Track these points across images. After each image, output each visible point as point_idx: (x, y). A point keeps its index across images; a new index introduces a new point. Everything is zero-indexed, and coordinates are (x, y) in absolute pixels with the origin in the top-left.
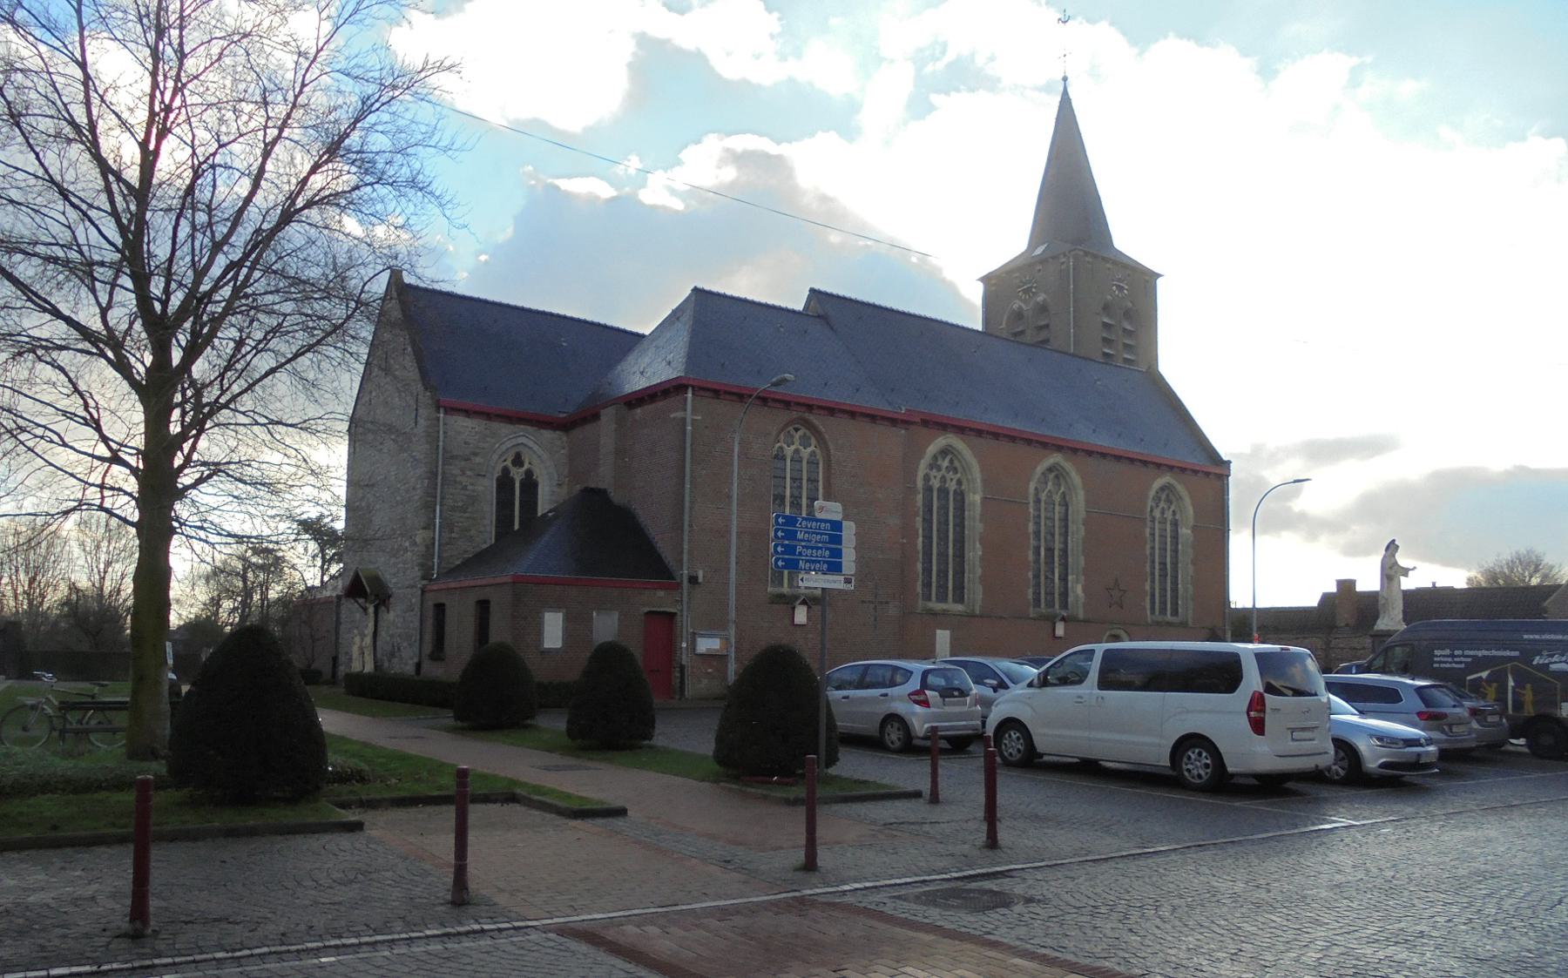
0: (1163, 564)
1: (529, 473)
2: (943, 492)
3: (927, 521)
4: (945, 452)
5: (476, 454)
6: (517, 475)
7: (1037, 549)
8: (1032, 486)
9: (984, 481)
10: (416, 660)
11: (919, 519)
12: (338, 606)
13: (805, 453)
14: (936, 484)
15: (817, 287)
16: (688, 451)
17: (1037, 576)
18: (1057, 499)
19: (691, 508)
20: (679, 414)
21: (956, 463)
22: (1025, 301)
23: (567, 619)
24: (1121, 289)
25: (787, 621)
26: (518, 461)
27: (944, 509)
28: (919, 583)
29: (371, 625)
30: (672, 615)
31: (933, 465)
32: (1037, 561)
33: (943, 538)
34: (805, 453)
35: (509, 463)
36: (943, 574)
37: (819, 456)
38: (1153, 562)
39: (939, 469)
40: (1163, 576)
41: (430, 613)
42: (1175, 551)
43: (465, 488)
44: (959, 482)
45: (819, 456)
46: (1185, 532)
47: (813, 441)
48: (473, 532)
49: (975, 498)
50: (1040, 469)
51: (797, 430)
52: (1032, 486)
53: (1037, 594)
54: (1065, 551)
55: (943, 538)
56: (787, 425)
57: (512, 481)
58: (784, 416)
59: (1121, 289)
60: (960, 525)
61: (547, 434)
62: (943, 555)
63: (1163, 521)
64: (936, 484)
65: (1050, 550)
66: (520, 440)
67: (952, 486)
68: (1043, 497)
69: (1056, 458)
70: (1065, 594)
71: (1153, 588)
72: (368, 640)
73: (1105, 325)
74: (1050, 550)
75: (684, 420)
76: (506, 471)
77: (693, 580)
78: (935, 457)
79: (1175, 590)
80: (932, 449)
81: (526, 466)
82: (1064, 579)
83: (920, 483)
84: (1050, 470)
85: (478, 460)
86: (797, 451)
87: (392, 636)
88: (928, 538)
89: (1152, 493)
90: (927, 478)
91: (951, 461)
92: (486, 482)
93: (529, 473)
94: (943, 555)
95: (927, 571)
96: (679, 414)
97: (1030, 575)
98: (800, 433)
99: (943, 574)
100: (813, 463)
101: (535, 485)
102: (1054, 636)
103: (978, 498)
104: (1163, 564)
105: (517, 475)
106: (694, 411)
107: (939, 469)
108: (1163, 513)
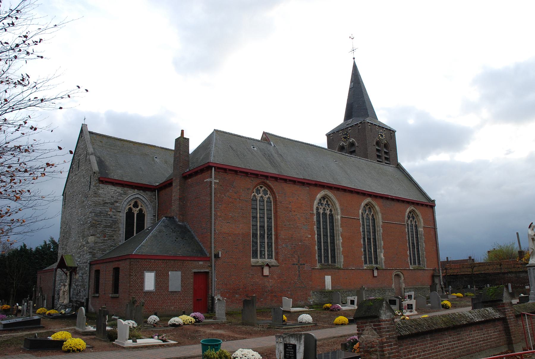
0: (413, 243)
1: (141, 210)
2: (324, 214)
3: (319, 228)
4: (324, 198)
5: (117, 202)
6: (136, 211)
7: (364, 238)
8: (360, 211)
9: (341, 209)
10: (87, 297)
11: (315, 227)
12: (56, 271)
13: (266, 198)
14: (321, 211)
15: (265, 131)
16: (213, 195)
17: (365, 251)
18: (371, 217)
19: (215, 224)
20: (208, 180)
21: (329, 203)
22: (345, 142)
23: (157, 277)
24: (382, 136)
25: (260, 274)
26: (136, 205)
27: (325, 222)
28: (317, 255)
29: (68, 281)
30: (207, 273)
31: (320, 203)
32: (364, 244)
33: (326, 235)
34: (266, 198)
35: (131, 206)
36: (326, 250)
37: (272, 199)
38: (409, 242)
39: (322, 204)
40: (414, 248)
41: (93, 275)
42: (417, 238)
43: (111, 217)
44: (331, 211)
45: (272, 199)
46: (421, 229)
47: (269, 192)
48: (115, 237)
49: (338, 217)
50: (363, 204)
51: (261, 187)
52: (360, 211)
53: (365, 258)
54: (375, 239)
55: (326, 235)
56: (257, 185)
57: (134, 214)
58: (258, 181)
59: (382, 136)
60: (332, 229)
61: (149, 193)
62: (326, 242)
63: (412, 225)
64: (321, 211)
65: (369, 239)
66: (137, 196)
67: (328, 212)
68: (365, 216)
69: (368, 200)
70: (376, 258)
71: (410, 254)
72: (67, 288)
73: (378, 150)
74: (369, 239)
75: (211, 182)
76: (130, 209)
77: (216, 256)
78: (320, 200)
79: (418, 254)
80: (319, 196)
81: (140, 207)
82: (375, 251)
83: (315, 212)
84: (367, 205)
85: (118, 204)
86: (262, 197)
87: (77, 286)
88: (319, 235)
89: (407, 214)
90: (317, 209)
91: (327, 202)
92: (121, 214)
93: (141, 210)
94: (326, 242)
95: (320, 249)
96: (208, 180)
97: (362, 250)
98: (263, 189)
99: (326, 250)
100: (269, 202)
101: (144, 215)
102: (374, 277)
103: (339, 217)
104: (413, 243)
105: (136, 211)
106: (215, 178)
107: (322, 204)
108: (411, 222)
